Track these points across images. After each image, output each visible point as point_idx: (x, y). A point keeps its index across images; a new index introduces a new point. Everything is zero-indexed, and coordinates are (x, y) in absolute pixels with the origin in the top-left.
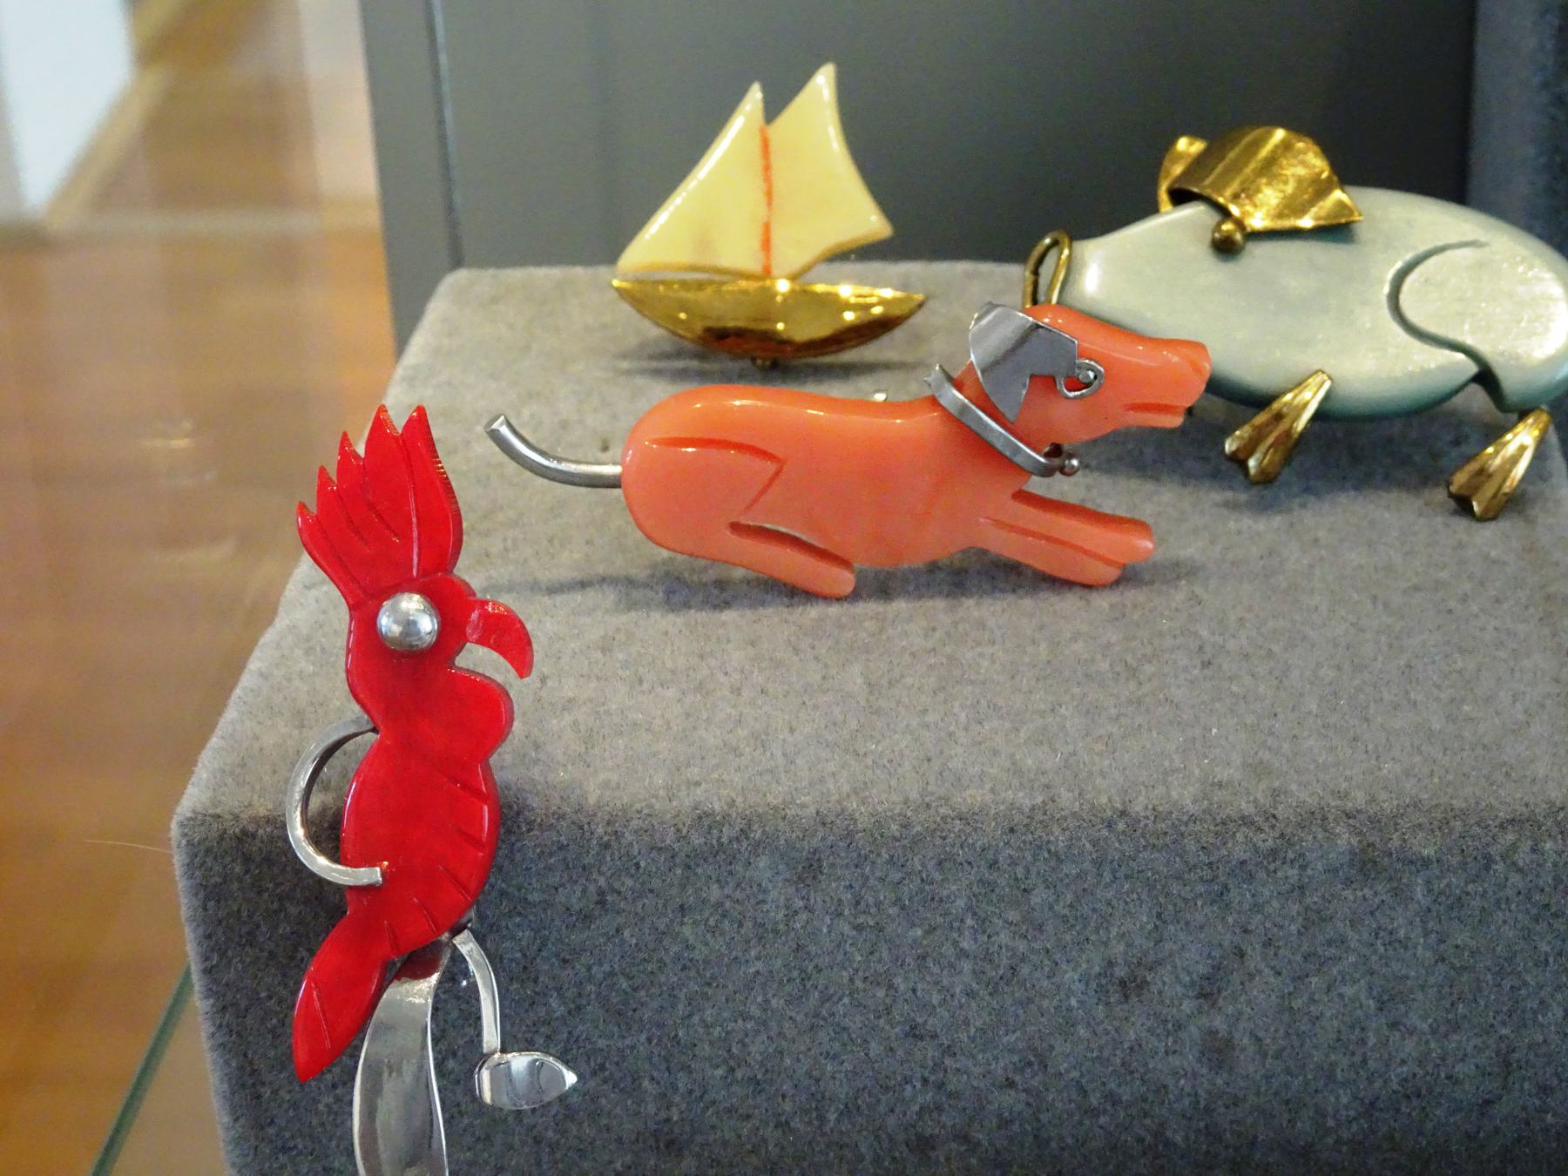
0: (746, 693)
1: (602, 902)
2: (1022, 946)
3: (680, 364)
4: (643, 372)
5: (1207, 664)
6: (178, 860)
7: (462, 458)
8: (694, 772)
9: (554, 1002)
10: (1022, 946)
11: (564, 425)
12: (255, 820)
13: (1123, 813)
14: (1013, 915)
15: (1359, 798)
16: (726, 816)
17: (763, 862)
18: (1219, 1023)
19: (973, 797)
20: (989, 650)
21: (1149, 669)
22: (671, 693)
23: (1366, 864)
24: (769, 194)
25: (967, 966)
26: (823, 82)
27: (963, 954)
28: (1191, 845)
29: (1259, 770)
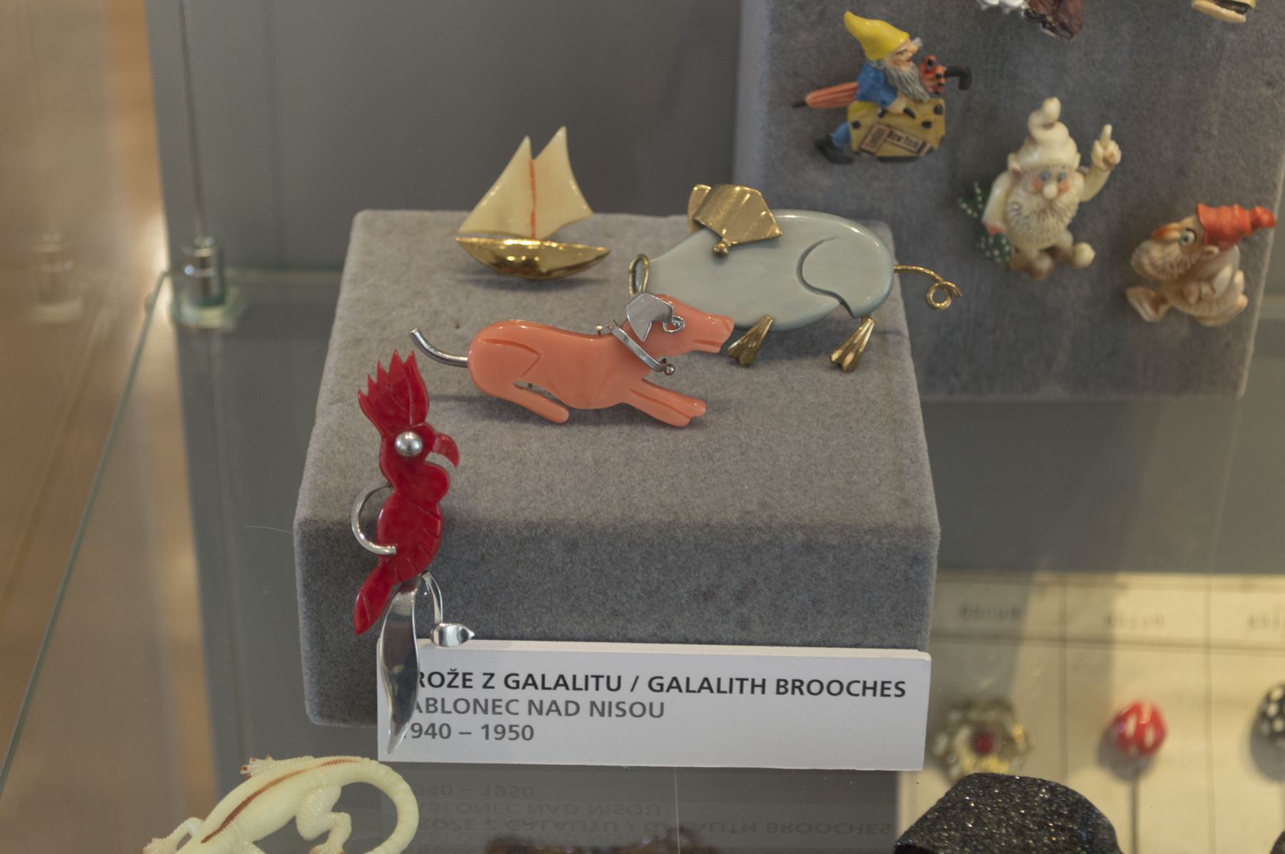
0: (542, 465)
1: (483, 558)
2: (662, 578)
3: (486, 277)
4: (470, 281)
5: (742, 454)
6: (296, 540)
7: (430, 376)
8: (523, 503)
9: (459, 599)
10: (662, 578)
11: (436, 313)
12: (332, 523)
13: (707, 525)
14: (659, 566)
15: (807, 520)
16: (539, 524)
17: (553, 543)
18: (745, 611)
19: (644, 516)
20: (646, 444)
21: (718, 455)
22: (508, 464)
23: (808, 547)
24: (534, 197)
25: (638, 586)
26: (561, 134)
27: (637, 581)
28: (735, 539)
29: (764, 505)
